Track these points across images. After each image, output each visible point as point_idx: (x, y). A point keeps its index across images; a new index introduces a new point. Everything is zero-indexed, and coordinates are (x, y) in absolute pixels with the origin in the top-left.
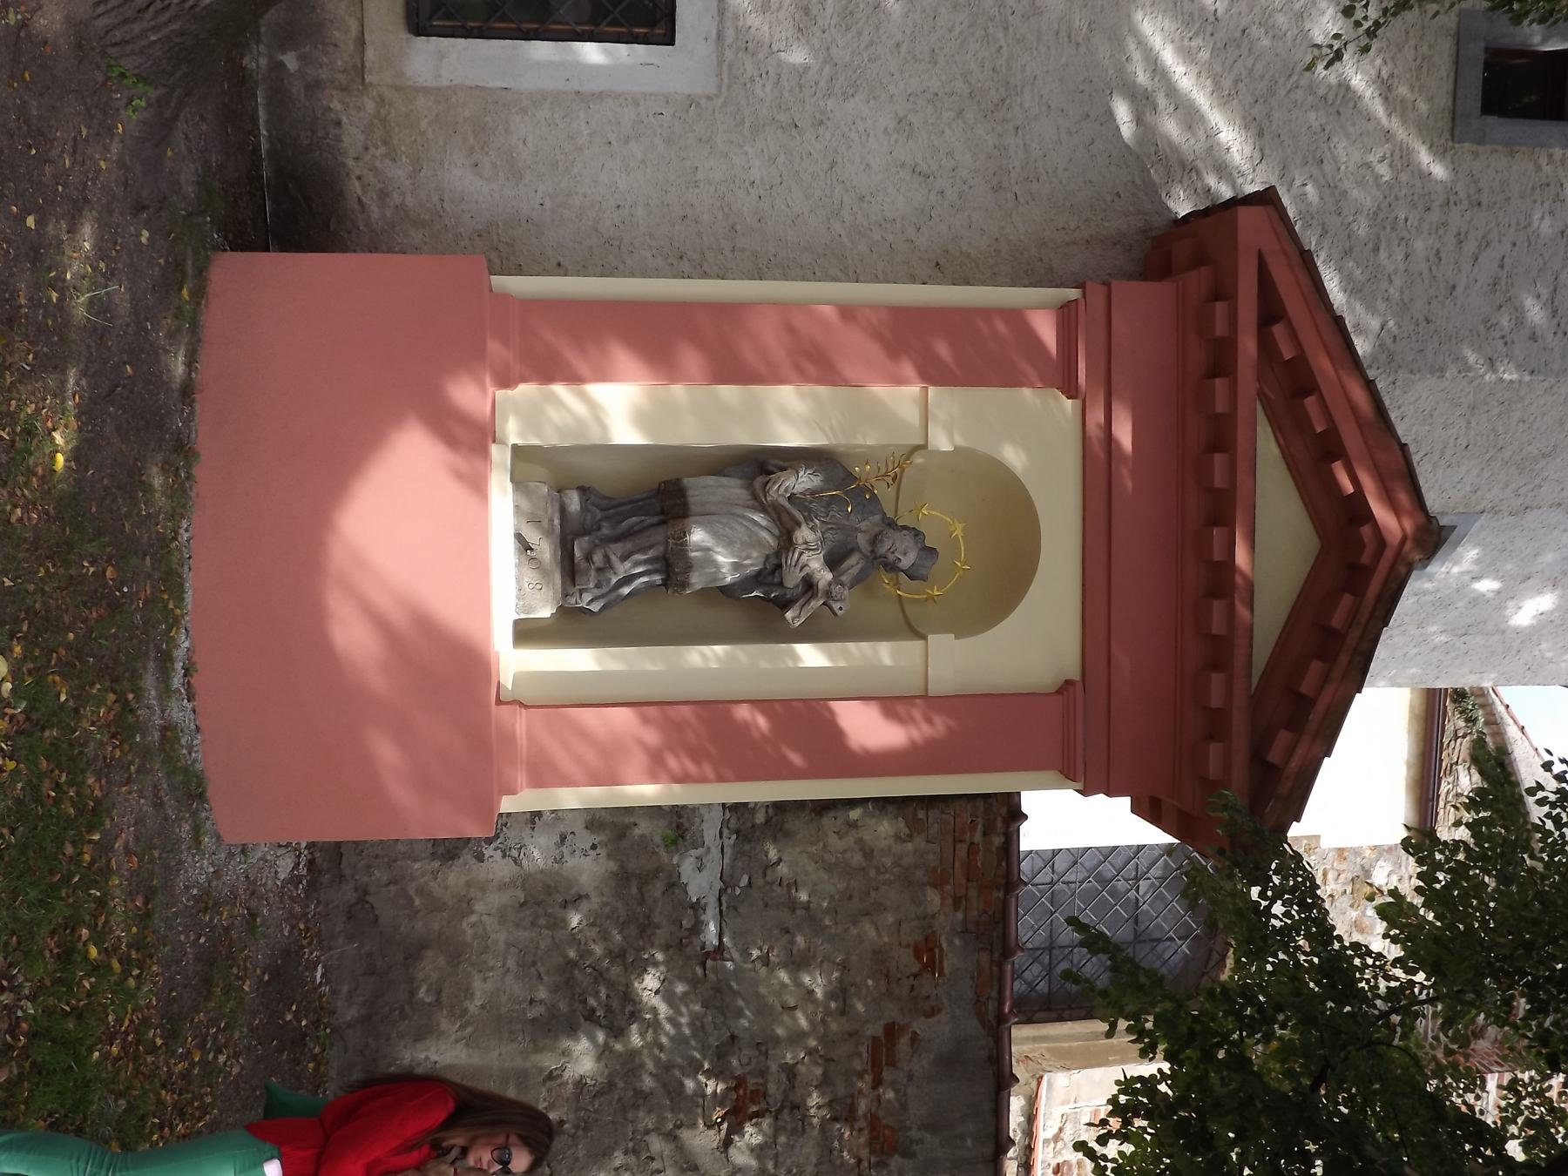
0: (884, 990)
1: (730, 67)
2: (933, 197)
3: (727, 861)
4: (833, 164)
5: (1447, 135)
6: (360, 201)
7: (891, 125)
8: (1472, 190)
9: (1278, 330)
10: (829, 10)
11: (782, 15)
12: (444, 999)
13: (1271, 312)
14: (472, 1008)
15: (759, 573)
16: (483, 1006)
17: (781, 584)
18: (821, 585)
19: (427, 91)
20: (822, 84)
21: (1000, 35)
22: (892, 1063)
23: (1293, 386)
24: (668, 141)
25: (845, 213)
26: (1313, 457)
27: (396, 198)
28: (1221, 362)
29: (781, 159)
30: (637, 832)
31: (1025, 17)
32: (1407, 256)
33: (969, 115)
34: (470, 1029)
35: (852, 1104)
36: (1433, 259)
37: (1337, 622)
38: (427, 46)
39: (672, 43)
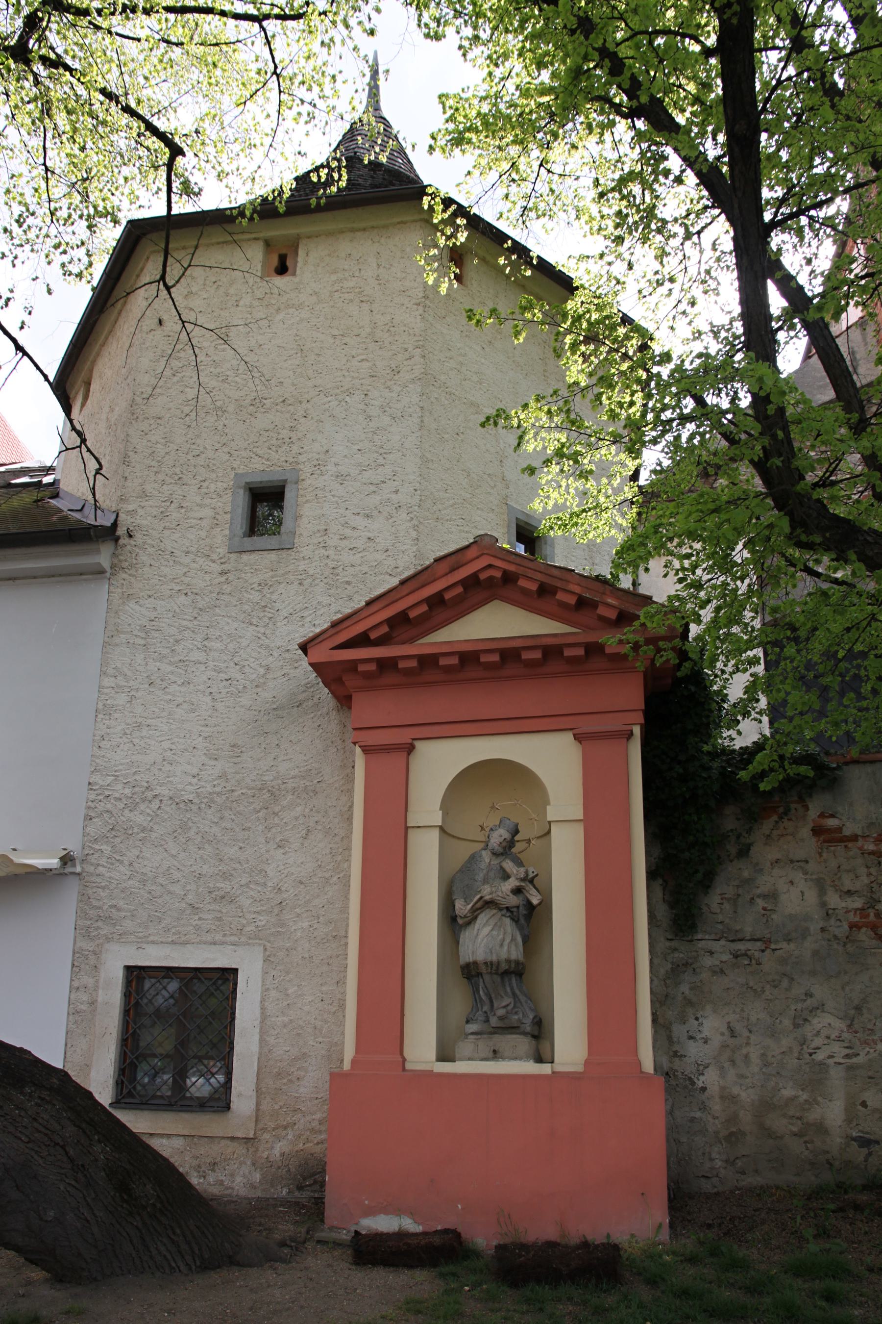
0: (790, 837)
1: (250, 938)
2: (320, 827)
3: (707, 937)
4: (301, 882)
5: (290, 552)
6: (318, 1143)
7: (282, 851)
8: (318, 535)
9: (373, 635)
10: (222, 885)
11: (224, 911)
12: (798, 1114)
13: (362, 640)
14: (805, 1097)
15: (512, 919)
16: (802, 1090)
17: (518, 907)
18: (518, 884)
19: (258, 1104)
20: (259, 889)
21: (236, 794)
22: (839, 829)
23: (401, 625)
24: (288, 973)
25: (327, 875)
26: (443, 607)
27: (315, 1124)
28: (386, 665)
29: (298, 910)
30: (687, 992)
31: (227, 780)
32: (352, 566)
33: (277, 809)
34: (819, 1099)
35: (869, 854)
36: (354, 551)
37: (534, 587)
38: (236, 1102)
39: (237, 970)
